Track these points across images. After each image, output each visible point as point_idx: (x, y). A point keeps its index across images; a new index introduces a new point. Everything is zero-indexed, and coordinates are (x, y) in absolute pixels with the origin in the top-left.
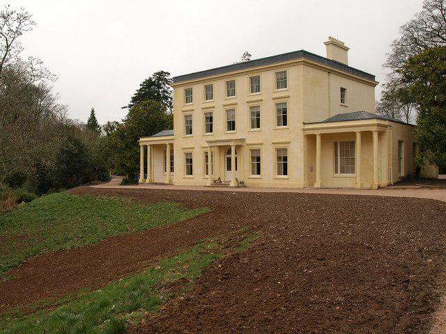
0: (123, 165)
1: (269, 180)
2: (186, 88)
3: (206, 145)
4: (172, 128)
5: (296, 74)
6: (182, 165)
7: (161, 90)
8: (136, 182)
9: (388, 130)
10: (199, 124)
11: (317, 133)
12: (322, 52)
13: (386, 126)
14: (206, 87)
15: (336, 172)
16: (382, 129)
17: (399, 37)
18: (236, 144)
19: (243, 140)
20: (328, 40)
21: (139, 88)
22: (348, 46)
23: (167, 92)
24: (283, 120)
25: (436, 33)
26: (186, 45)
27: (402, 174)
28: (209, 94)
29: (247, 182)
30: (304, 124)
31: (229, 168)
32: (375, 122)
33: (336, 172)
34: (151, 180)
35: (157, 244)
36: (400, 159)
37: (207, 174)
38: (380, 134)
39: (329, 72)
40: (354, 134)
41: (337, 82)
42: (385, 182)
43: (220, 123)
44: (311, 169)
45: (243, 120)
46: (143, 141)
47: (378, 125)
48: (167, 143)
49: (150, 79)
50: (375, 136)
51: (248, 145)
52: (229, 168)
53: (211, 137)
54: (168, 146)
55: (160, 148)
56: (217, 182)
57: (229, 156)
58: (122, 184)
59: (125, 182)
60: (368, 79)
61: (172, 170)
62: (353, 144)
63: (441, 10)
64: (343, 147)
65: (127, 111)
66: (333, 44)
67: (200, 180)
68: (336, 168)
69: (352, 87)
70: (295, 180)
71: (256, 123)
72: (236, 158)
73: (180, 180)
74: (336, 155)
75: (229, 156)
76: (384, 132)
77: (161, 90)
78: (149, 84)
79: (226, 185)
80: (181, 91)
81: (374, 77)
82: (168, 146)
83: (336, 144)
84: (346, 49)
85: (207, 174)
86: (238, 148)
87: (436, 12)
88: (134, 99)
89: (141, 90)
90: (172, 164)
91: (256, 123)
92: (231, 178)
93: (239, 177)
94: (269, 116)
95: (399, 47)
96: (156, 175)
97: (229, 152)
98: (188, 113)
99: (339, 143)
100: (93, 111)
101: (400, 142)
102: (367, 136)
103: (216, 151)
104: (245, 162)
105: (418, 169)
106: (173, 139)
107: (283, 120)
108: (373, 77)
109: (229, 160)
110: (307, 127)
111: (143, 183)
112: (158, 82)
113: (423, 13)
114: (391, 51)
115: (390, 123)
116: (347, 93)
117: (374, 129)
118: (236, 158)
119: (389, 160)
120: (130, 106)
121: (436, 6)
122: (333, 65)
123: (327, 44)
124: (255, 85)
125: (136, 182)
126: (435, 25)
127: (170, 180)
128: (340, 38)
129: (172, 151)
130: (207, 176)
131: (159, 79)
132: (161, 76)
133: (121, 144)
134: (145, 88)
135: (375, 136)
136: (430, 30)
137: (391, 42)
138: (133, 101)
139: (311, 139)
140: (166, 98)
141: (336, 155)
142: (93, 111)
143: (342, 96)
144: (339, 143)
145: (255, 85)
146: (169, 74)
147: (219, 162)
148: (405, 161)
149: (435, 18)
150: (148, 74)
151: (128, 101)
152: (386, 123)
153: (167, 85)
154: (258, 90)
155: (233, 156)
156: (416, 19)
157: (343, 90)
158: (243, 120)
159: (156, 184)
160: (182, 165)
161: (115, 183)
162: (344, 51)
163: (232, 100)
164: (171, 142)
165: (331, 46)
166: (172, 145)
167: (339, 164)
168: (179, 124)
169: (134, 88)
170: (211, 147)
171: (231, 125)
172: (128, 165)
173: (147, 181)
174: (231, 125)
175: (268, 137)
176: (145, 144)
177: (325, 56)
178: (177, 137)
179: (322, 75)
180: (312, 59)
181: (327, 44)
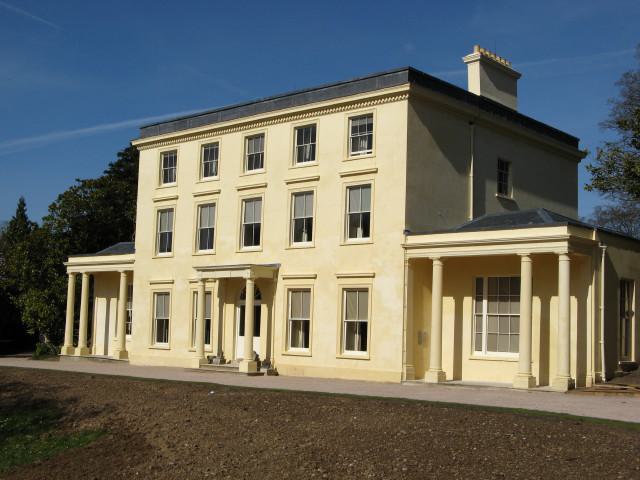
1: (322, 362)
3: (197, 276)
11: (434, 254)
19: (275, 269)
21: (115, 159)
24: (360, 224)
33: (479, 348)
40: (514, 260)
43: (228, 231)
44: (417, 338)
45: (276, 223)
48: (120, 268)
53: (207, 258)
67: (181, 355)
71: (303, 229)
73: (144, 355)
83: (479, 282)
90: (128, 318)
91: (303, 229)
94: (330, 215)
100: (22, 204)
102: (545, 265)
107: (360, 224)
125: (56, 355)
142: (22, 204)
158: (276, 223)
164: (128, 267)
166: (130, 275)
171: (252, 235)
174: (252, 235)
176: (82, 270)
178: (143, 261)
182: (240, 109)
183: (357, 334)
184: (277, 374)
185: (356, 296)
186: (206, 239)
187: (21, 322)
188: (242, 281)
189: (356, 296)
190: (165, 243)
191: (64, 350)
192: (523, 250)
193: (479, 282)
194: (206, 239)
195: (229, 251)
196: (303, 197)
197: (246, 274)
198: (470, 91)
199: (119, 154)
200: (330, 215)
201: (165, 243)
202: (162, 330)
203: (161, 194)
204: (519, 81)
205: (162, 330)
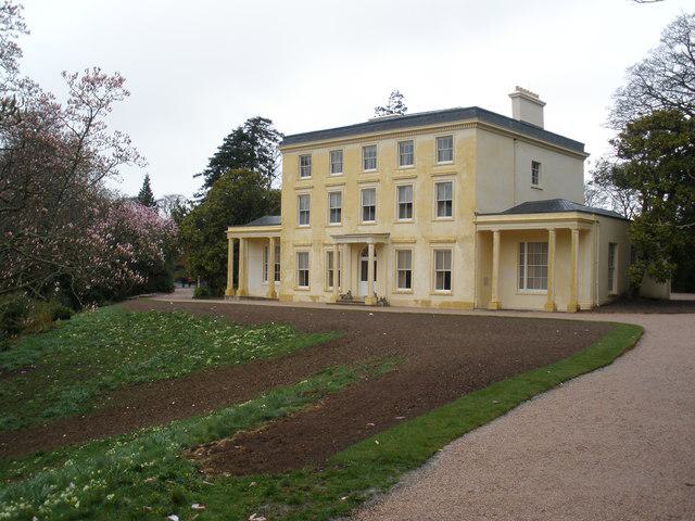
0: (200, 268)
1: (423, 294)
2: (302, 153)
3: (334, 242)
4: (278, 212)
5: (465, 138)
6: (296, 267)
7: (256, 148)
8: (221, 295)
9: (594, 228)
10: (320, 210)
11: (495, 228)
12: (506, 109)
13: (591, 222)
14: (332, 153)
15: (522, 287)
16: (585, 226)
17: (625, 84)
18: (376, 241)
20: (513, 91)
21: (222, 143)
22: (544, 101)
23: (266, 151)
24: (445, 207)
25: (681, 80)
26: (313, 93)
27: (615, 291)
28: (336, 164)
29: (392, 299)
30: (477, 214)
31: (364, 277)
32: (574, 215)
33: (522, 287)
34: (243, 292)
35: (256, 373)
36: (611, 270)
37: (331, 285)
38: (583, 234)
39: (516, 138)
40: (545, 232)
41: (527, 153)
42: (586, 303)
43: (352, 206)
44: (485, 281)
45: (387, 204)
46: (233, 232)
47: (580, 220)
48: (270, 235)
49: (240, 130)
50: (575, 236)
51: (393, 243)
52: (364, 277)
54: (272, 242)
55: (260, 243)
56: (347, 299)
57: (364, 259)
58: (196, 297)
59: (201, 295)
60: (575, 150)
61: (277, 277)
62: (546, 245)
63: (688, 45)
64: (531, 250)
65: (202, 180)
66: (524, 98)
67: (319, 294)
68: (522, 280)
69: (548, 160)
70: (463, 293)
71: (406, 209)
72: (375, 263)
73: (291, 293)
74: (522, 262)
75: (364, 259)
76: (588, 231)
77: (256, 148)
78: (238, 137)
79: (361, 304)
80: (294, 157)
81: (542, 105)
82: (272, 242)
83: (522, 245)
84: (542, 105)
85: (331, 285)
86: (379, 247)
87: (680, 48)
88: (214, 162)
89: (224, 147)
90: (277, 268)
91: (406, 209)
92: (365, 291)
93: (382, 286)
94: (424, 198)
95: (625, 98)
96: (253, 281)
97: (365, 253)
98: (304, 192)
99: (496, 237)
100: (147, 180)
101: (612, 246)
102: (563, 235)
103: (345, 250)
104: (388, 269)
105: (637, 290)
106: (280, 231)
107: (445, 207)
108: (580, 146)
109: (365, 265)
110: (480, 219)
111: (231, 298)
112: (253, 133)
113: (661, 49)
114: (614, 105)
115: (598, 218)
116: (542, 170)
117: (574, 226)
118: (375, 263)
119: (594, 270)
120: (207, 173)
121: (679, 40)
122: (522, 130)
123: (512, 96)
124: (406, 155)
125: (221, 295)
126: (678, 68)
127: (274, 293)
128: (531, 87)
129: (278, 249)
130: (331, 288)
131: (254, 130)
132: (258, 125)
133: (198, 235)
134: (232, 145)
135: (575, 236)
136: (671, 75)
137: (614, 91)
138: (211, 165)
139: (486, 237)
140: (264, 160)
141: (522, 262)
142: (147, 180)
143: (535, 173)
144: (496, 237)
145: (406, 155)
146: (270, 122)
147: (348, 268)
148: (620, 272)
149: (678, 58)
150: (237, 121)
151: (204, 165)
152: (592, 218)
153: (266, 140)
154: (411, 161)
155: (371, 259)
156: (650, 57)
157: (535, 165)
158: (387, 204)
159: (253, 298)
160: (296, 267)
161: (184, 294)
162: (538, 107)
163: (371, 173)
164: (277, 234)
165: (518, 100)
166: (277, 240)
167: (525, 275)
168: (289, 207)
169: (213, 145)
170: (338, 244)
171: (369, 212)
172: (209, 268)
173: (238, 293)
174: (369, 212)
175: (420, 233)
176: (239, 236)
177: (510, 116)
178: (288, 230)
179: (505, 144)
180: (493, 121)
181: (512, 96)
182: (382, 125)
183: (445, 280)
184: (389, 306)
185: (443, 256)
186: (336, 214)
187: (652, 215)
188: (367, 245)
189: (443, 256)
190: (304, 216)
191: (227, 292)
192: (550, 227)
193: (522, 245)
194: (336, 214)
195: (353, 224)
196: (444, 187)
197: (369, 241)
198: (546, 128)
199: (225, 140)
200: (424, 198)
201: (304, 216)
202: (304, 278)
203: (331, 181)
204: (545, 108)
205: (304, 278)
